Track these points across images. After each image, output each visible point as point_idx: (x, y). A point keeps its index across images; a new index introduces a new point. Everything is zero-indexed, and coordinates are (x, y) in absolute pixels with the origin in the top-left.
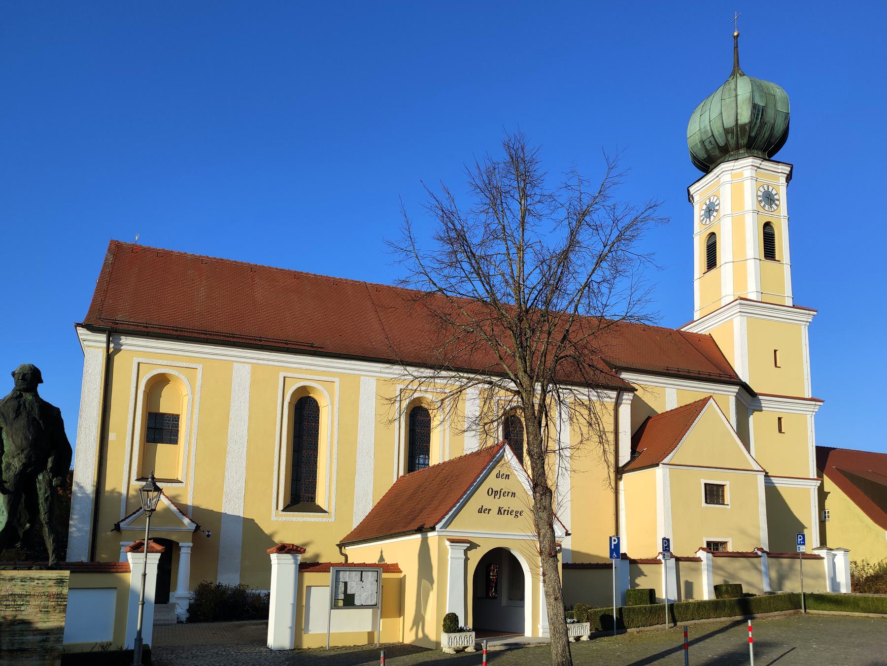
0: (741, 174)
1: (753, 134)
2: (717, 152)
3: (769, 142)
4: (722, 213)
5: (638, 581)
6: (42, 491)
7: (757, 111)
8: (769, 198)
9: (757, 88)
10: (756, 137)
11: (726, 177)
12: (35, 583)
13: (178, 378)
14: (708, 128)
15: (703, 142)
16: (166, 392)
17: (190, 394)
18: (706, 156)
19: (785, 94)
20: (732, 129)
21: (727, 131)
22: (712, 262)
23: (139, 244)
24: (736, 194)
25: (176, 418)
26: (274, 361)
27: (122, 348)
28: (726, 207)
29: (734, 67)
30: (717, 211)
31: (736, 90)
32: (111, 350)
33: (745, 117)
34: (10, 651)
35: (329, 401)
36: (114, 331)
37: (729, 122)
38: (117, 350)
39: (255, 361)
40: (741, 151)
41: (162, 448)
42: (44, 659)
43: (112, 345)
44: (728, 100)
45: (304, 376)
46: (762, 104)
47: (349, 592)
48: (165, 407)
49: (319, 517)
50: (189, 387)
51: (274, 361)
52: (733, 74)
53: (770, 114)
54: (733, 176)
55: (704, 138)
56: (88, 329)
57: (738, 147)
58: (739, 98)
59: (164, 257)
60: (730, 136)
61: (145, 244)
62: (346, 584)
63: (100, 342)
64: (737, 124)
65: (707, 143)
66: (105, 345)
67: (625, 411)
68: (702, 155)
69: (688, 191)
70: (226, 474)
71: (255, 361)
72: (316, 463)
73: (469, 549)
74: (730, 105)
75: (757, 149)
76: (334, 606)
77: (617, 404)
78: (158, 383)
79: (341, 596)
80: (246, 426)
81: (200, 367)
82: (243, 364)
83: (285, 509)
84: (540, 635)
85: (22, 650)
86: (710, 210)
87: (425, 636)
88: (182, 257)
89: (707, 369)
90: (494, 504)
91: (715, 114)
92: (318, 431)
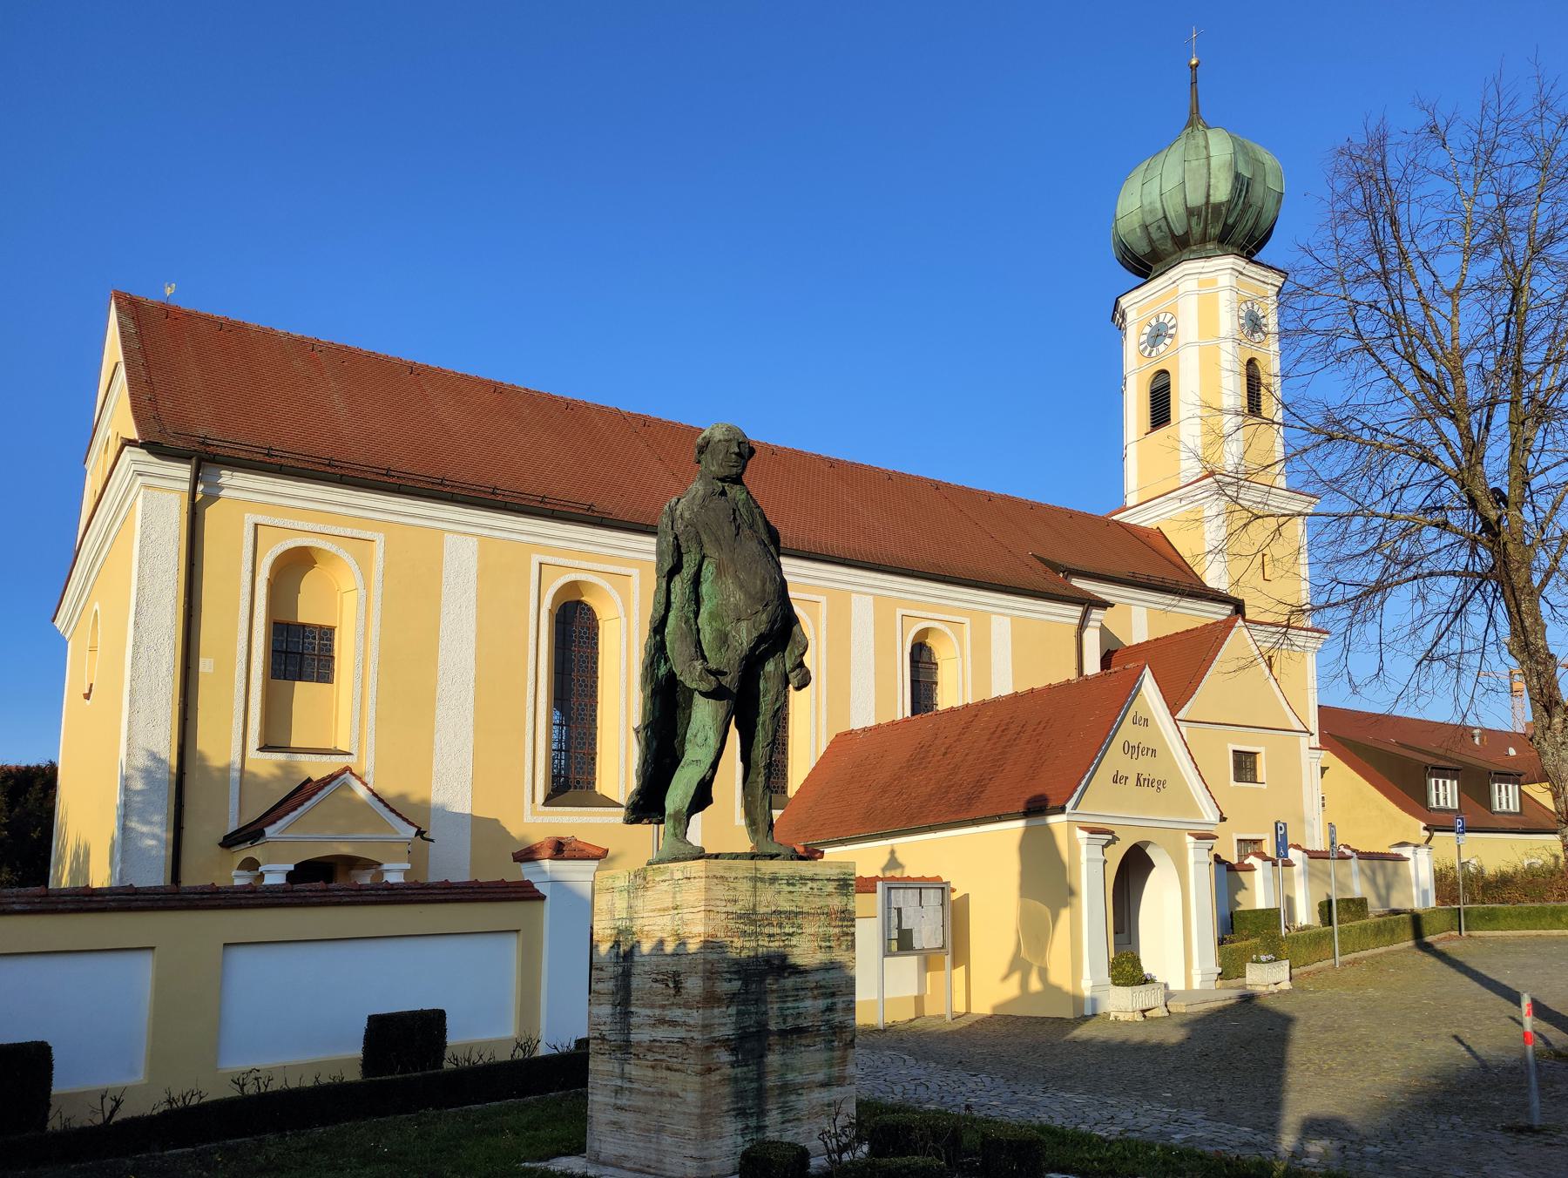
0: (1214, 281)
1: (1230, 221)
2: (1169, 245)
3: (1250, 237)
4: (1181, 339)
5: (1240, 897)
6: (769, 697)
7: (1241, 185)
8: (1254, 324)
9: (1240, 149)
10: (1233, 226)
11: (1190, 284)
12: (806, 889)
13: (334, 556)
14: (1158, 205)
15: (1145, 227)
16: (310, 585)
17: (361, 586)
18: (1148, 250)
19: (1277, 163)
20: (1199, 209)
21: (1191, 212)
22: (1160, 413)
23: (173, 303)
24: (1202, 314)
25: (327, 634)
26: (521, 533)
27: (223, 493)
28: (1188, 328)
29: (1192, 113)
30: (1171, 336)
31: (1207, 147)
32: (199, 497)
33: (1222, 192)
34: (783, 1033)
35: (621, 609)
36: (205, 460)
37: (1196, 199)
38: (212, 498)
39: (486, 532)
40: (1210, 246)
41: (303, 691)
42: (832, 1049)
43: (200, 487)
44: (1194, 163)
45: (576, 563)
46: (1247, 175)
47: (904, 927)
48: (308, 613)
49: (609, 814)
50: (358, 574)
51: (521, 533)
52: (1190, 124)
53: (1258, 191)
54: (1201, 284)
55: (1149, 220)
56: (151, 452)
57: (1204, 239)
58: (1213, 162)
59: (230, 333)
60: (1194, 220)
61: (188, 305)
62: (899, 910)
63: (175, 479)
64: (1207, 202)
65: (1152, 230)
66: (186, 486)
67: (1092, 639)
68: (1142, 248)
69: (1117, 302)
70: (437, 737)
71: (486, 532)
72: (594, 720)
73: (1109, 843)
74: (1186, 173)
75: (1232, 244)
76: (888, 953)
77: (1082, 627)
78: (294, 566)
79: (895, 934)
80: (472, 651)
81: (380, 538)
82: (463, 538)
83: (549, 800)
84: (1196, 985)
85: (799, 1031)
86: (1158, 335)
87: (1051, 990)
88: (267, 335)
89: (1171, 577)
90: (1131, 767)
91: (1171, 183)
92: (596, 663)
